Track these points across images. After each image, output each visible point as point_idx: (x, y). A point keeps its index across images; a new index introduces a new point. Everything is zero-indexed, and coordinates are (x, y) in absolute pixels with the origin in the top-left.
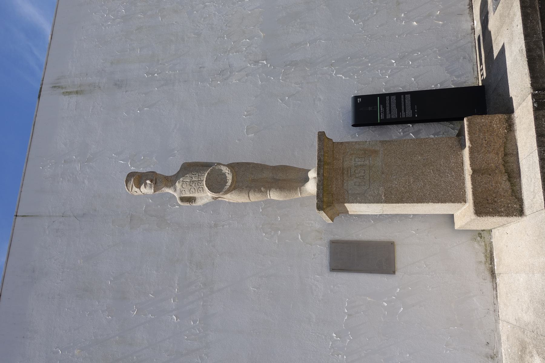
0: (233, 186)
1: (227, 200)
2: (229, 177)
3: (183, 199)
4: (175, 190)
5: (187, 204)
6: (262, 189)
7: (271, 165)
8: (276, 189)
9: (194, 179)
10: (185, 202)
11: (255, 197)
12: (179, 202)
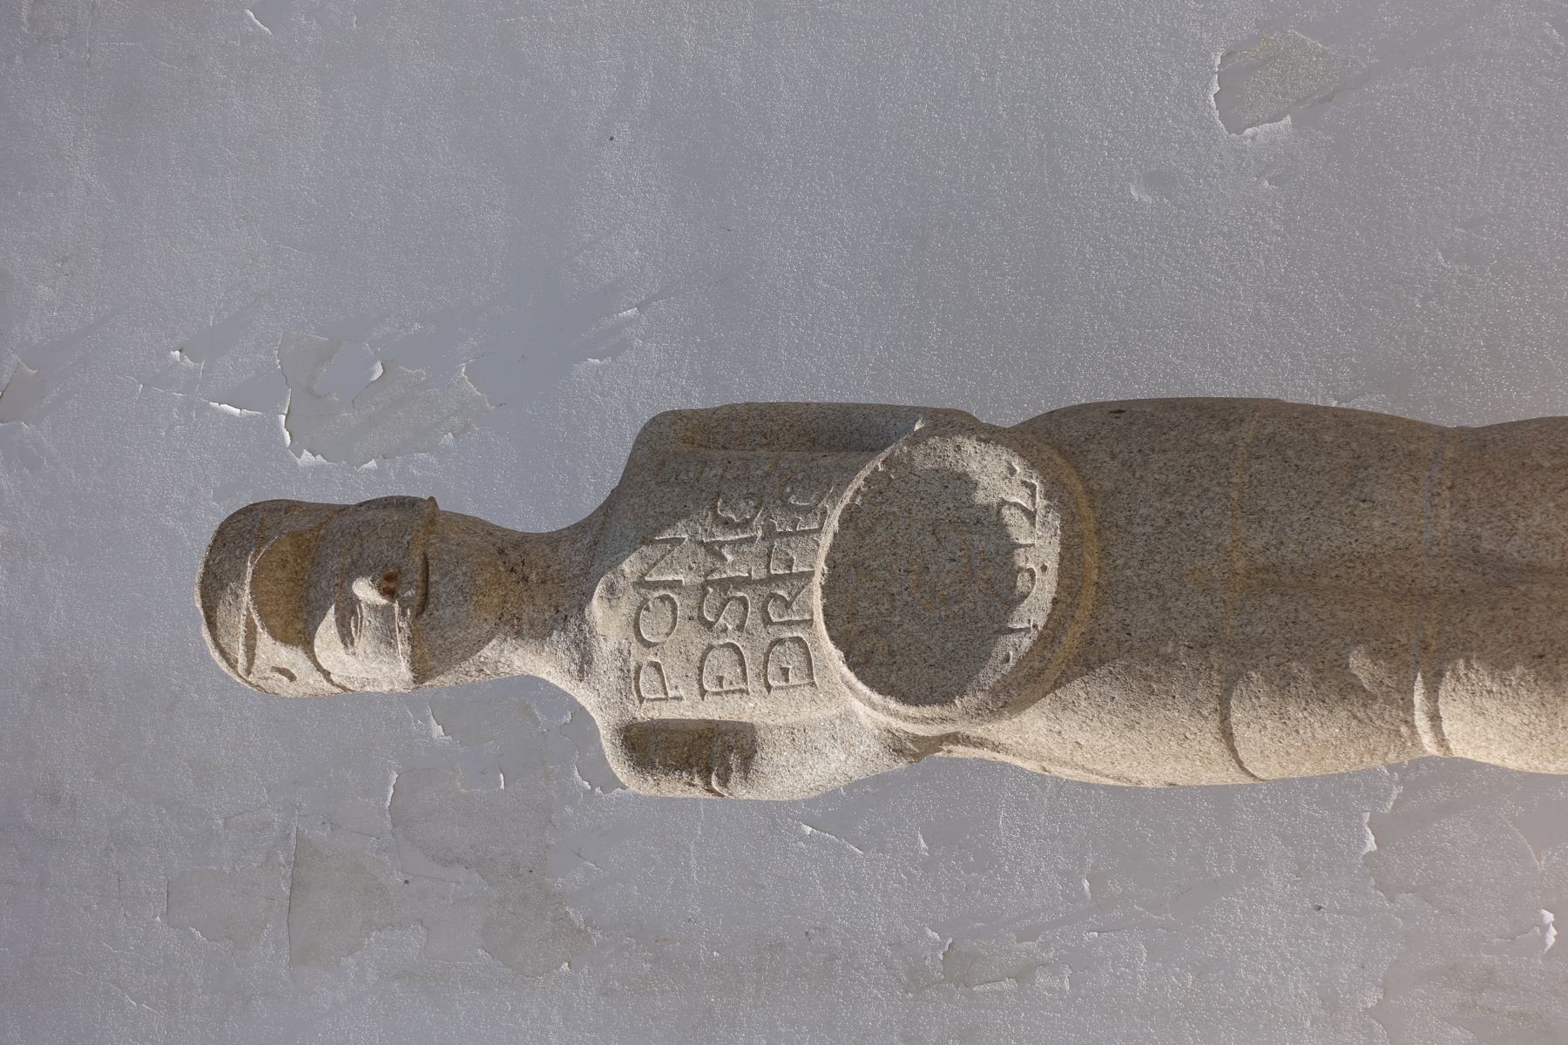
0: (1071, 639)
1: (1030, 766)
2: (1038, 549)
3: (650, 745)
4: (584, 666)
5: (677, 789)
6: (1360, 665)
7: (1451, 421)
8: (1500, 666)
9: (734, 566)
10: (668, 768)
11: (1285, 743)
12: (620, 769)
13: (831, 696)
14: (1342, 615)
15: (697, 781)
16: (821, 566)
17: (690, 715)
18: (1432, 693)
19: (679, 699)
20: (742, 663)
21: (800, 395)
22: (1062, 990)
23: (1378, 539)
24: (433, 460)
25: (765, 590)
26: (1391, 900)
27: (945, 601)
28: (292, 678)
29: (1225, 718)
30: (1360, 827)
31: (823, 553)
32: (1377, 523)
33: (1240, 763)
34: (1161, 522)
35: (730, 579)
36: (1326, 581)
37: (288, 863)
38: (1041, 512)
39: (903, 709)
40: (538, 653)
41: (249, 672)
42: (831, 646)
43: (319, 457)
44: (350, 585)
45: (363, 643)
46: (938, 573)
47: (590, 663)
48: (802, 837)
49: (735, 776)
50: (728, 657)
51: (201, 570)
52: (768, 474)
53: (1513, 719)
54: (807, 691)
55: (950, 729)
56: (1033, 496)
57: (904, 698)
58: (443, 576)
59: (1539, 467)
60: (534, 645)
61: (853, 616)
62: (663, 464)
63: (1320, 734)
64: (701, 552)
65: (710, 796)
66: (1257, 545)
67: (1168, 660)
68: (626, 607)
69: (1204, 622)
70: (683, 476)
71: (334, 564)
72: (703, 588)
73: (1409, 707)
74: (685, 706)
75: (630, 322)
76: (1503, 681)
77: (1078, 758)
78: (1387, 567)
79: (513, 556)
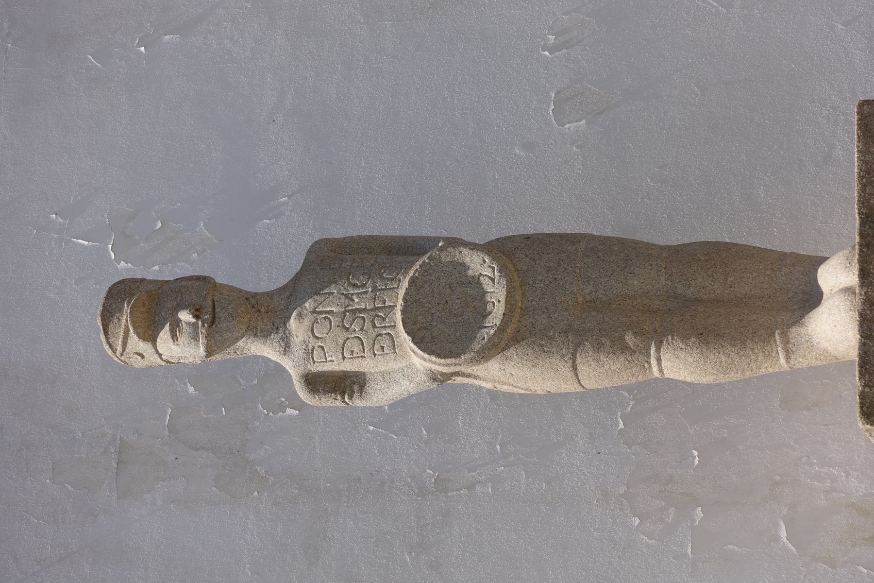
0: (510, 330)
2: (497, 294)
3: (316, 382)
4: (286, 348)
6: (630, 339)
8: (685, 338)
9: (358, 303)
11: (599, 373)
12: (303, 394)
13: (403, 357)
14: (622, 319)
15: (339, 397)
16: (400, 301)
17: (337, 368)
18: (658, 350)
19: (333, 361)
20: (362, 345)
21: (384, 232)
22: (488, 493)
23: (636, 289)
24: (187, 266)
25: (374, 313)
26: (630, 449)
27: (455, 315)
28: (143, 357)
29: (574, 361)
30: (616, 418)
31: (401, 297)
32: (635, 282)
33: (579, 381)
34: (547, 282)
35: (357, 309)
36: (614, 306)
37: (115, 452)
38: (497, 278)
39: (438, 360)
40: (264, 344)
41: (122, 355)
42: (406, 335)
43: (129, 265)
44: (177, 314)
45: (183, 339)
46: (452, 304)
47: (289, 347)
48: (368, 431)
49: (356, 395)
50: (356, 342)
51: (101, 308)
52: (372, 265)
53: (690, 360)
54: (392, 356)
55: (458, 369)
56: (494, 272)
57: (439, 356)
58: (222, 309)
59: (700, 260)
60: (262, 340)
61: (415, 323)
62: (322, 261)
63: (613, 367)
64: (343, 298)
65: (343, 405)
66: (587, 291)
67: (551, 338)
68: (307, 322)
69: (566, 323)
70: (333, 266)
71: (169, 305)
72: (344, 313)
73: (649, 356)
74: (335, 364)
75: (284, 203)
76: (686, 344)
77: (511, 381)
78: (639, 301)
79: (253, 301)
